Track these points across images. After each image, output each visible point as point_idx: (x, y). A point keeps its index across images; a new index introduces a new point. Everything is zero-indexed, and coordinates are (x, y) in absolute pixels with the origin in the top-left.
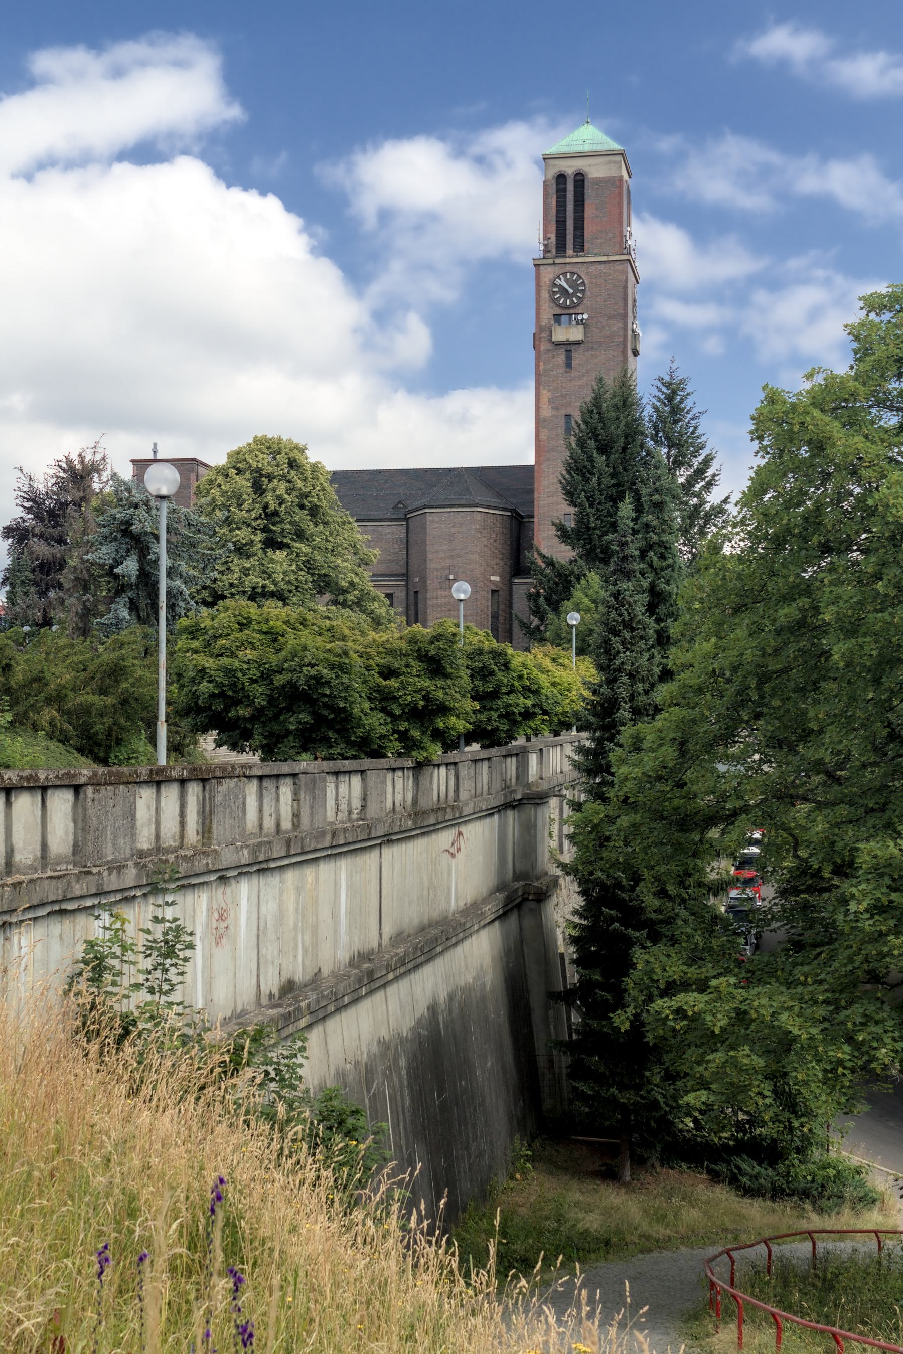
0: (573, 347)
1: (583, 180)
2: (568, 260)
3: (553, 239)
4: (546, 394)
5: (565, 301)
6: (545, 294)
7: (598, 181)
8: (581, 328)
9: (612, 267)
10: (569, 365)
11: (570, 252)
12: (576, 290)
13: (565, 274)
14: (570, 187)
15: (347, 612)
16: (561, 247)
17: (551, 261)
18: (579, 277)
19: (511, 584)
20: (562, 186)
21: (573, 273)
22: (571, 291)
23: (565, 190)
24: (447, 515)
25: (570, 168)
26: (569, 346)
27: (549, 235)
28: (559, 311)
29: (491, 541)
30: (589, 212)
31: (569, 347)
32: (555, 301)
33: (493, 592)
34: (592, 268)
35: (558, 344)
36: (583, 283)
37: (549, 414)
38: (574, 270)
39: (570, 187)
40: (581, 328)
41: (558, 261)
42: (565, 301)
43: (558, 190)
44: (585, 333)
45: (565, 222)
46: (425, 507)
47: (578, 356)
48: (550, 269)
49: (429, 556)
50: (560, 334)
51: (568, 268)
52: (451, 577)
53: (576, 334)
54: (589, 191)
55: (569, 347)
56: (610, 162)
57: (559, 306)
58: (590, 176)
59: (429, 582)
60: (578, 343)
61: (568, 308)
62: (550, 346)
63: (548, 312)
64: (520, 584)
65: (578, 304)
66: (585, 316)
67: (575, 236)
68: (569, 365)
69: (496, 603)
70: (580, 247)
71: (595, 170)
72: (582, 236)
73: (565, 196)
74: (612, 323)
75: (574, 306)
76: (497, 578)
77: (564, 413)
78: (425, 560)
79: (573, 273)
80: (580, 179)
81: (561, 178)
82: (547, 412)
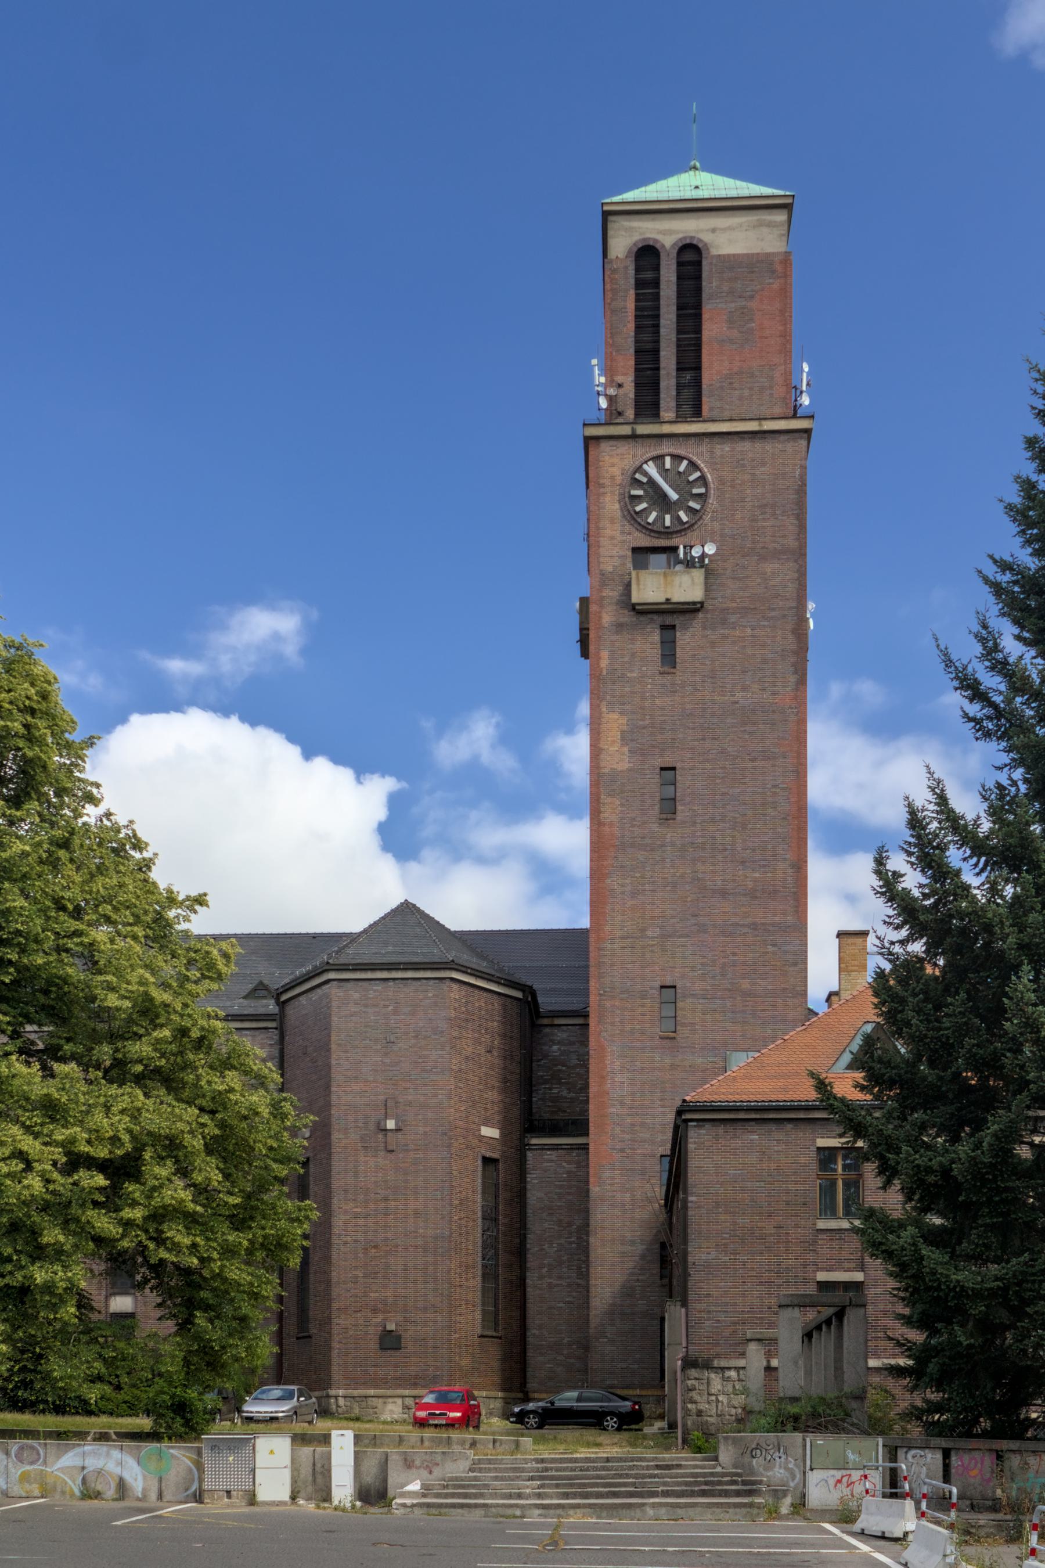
0: (677, 620)
1: (699, 263)
2: (666, 429)
3: (629, 389)
4: (615, 722)
5: (660, 519)
6: (611, 505)
7: (731, 263)
8: (698, 575)
9: (769, 447)
11: (667, 414)
12: (686, 494)
13: (658, 459)
14: (668, 274)
15: (129, 1096)
16: (647, 404)
17: (626, 430)
18: (693, 466)
19: (522, 1149)
20: (648, 275)
21: (677, 458)
22: (674, 496)
23: (656, 283)
24: (379, 987)
25: (667, 233)
26: (669, 617)
27: (619, 379)
28: (645, 541)
29: (481, 1049)
30: (712, 329)
31: (669, 620)
32: (634, 519)
33: (487, 1161)
34: (724, 448)
35: (643, 612)
36: (703, 479)
37: (624, 765)
38: (681, 452)
39: (668, 274)
40: (698, 575)
41: (642, 429)
42: (660, 519)
43: (639, 284)
44: (708, 588)
45: (656, 351)
46: (327, 968)
47: (687, 639)
48: (623, 448)
49: (337, 1075)
50: (652, 587)
51: (666, 448)
52: (391, 1124)
53: (687, 587)
54: (710, 283)
55: (669, 620)
56: (761, 224)
57: (648, 529)
58: (714, 252)
59: (335, 1136)
60: (691, 609)
61: (667, 533)
62: (627, 617)
63: (617, 540)
64: (543, 1147)
65: (690, 527)
66: (710, 549)
67: (679, 387)
69: (491, 1188)
70: (692, 404)
71: (728, 239)
72: (697, 384)
73: (657, 297)
74: (769, 567)
75: (683, 529)
76: (490, 1132)
77: (659, 762)
78: (328, 1087)
79: (677, 458)
80: (691, 253)
81: (647, 255)
82: (618, 759)
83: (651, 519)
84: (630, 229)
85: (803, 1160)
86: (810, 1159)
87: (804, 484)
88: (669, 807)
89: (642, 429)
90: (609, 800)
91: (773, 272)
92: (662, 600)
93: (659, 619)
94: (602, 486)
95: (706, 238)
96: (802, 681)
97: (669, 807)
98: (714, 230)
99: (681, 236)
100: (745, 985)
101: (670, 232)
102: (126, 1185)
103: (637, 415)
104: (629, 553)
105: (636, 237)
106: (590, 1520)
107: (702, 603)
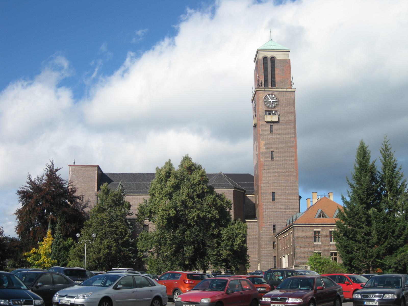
2: (270, 90)
10: (271, 131)
11: (270, 86)
16: (266, 85)
17: (263, 90)
25: (269, 55)
30: (277, 72)
35: (268, 122)
37: (264, 151)
41: (266, 90)
51: (270, 92)
53: (275, 119)
54: (277, 65)
61: (271, 108)
68: (271, 131)
70: (273, 85)
71: (279, 56)
80: (273, 59)
81: (265, 58)
83: (271, 106)
84: (262, 54)
85: (312, 233)
86: (312, 233)
87: (294, 100)
88: (272, 158)
89: (266, 90)
90: (262, 157)
91: (287, 63)
92: (271, 121)
93: (270, 124)
94: (259, 99)
95: (275, 56)
96: (295, 136)
97: (272, 158)
98: (277, 55)
99: (271, 55)
100: (287, 192)
101: (269, 55)
102: (207, 271)
103: (264, 86)
104: (264, 111)
105: (263, 55)
106: (197, 272)
107: (266, 114)
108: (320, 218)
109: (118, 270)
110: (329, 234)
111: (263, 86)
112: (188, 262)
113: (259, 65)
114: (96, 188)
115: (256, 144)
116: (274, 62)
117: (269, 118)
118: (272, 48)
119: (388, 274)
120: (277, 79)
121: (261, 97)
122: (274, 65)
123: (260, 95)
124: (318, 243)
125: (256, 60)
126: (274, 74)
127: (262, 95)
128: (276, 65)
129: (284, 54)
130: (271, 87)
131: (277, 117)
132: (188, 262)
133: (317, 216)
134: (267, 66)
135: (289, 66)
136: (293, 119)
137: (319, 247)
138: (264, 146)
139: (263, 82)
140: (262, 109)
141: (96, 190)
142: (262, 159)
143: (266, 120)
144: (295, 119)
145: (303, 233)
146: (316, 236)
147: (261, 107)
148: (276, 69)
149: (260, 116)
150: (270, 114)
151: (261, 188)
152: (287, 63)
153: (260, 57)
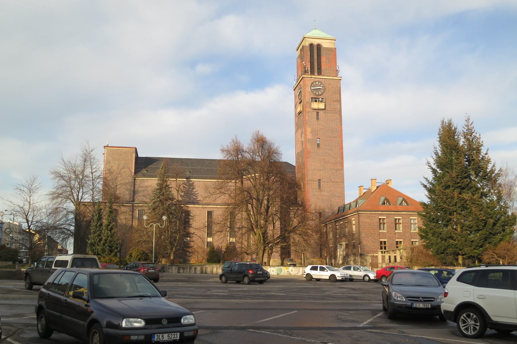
2: (317, 77)
17: (310, 76)
25: (315, 42)
30: (323, 59)
37: (311, 138)
41: (313, 76)
51: (317, 79)
53: (322, 106)
54: (322, 52)
68: (318, 118)
71: (325, 44)
80: (319, 46)
81: (311, 45)
84: (308, 41)
86: (378, 220)
108: (384, 206)
109: (15, 316)
110: (394, 222)
111: (310, 73)
112: (163, 263)
113: (305, 52)
114: (133, 171)
115: (300, 131)
116: (320, 50)
117: (315, 105)
118: (318, 36)
119: (127, 269)
120: (323, 67)
121: (308, 83)
122: (320, 53)
123: (306, 82)
124: (384, 231)
125: (301, 47)
126: (320, 62)
127: (308, 82)
128: (322, 53)
129: (331, 42)
130: (317, 74)
131: (324, 104)
132: (163, 263)
133: (381, 203)
134: (313, 53)
135: (335, 55)
136: (339, 107)
137: (384, 235)
138: (311, 133)
139: (309, 69)
140: (308, 97)
141: (133, 174)
142: (308, 146)
143: (312, 107)
144: (341, 107)
145: (368, 220)
146: (381, 223)
147: (307, 94)
148: (322, 57)
149: (307, 103)
150: (316, 101)
151: (307, 175)
152: (333, 52)
153: (307, 43)
